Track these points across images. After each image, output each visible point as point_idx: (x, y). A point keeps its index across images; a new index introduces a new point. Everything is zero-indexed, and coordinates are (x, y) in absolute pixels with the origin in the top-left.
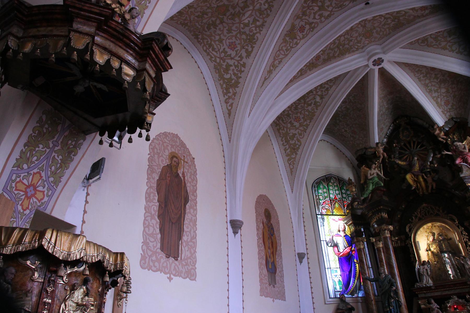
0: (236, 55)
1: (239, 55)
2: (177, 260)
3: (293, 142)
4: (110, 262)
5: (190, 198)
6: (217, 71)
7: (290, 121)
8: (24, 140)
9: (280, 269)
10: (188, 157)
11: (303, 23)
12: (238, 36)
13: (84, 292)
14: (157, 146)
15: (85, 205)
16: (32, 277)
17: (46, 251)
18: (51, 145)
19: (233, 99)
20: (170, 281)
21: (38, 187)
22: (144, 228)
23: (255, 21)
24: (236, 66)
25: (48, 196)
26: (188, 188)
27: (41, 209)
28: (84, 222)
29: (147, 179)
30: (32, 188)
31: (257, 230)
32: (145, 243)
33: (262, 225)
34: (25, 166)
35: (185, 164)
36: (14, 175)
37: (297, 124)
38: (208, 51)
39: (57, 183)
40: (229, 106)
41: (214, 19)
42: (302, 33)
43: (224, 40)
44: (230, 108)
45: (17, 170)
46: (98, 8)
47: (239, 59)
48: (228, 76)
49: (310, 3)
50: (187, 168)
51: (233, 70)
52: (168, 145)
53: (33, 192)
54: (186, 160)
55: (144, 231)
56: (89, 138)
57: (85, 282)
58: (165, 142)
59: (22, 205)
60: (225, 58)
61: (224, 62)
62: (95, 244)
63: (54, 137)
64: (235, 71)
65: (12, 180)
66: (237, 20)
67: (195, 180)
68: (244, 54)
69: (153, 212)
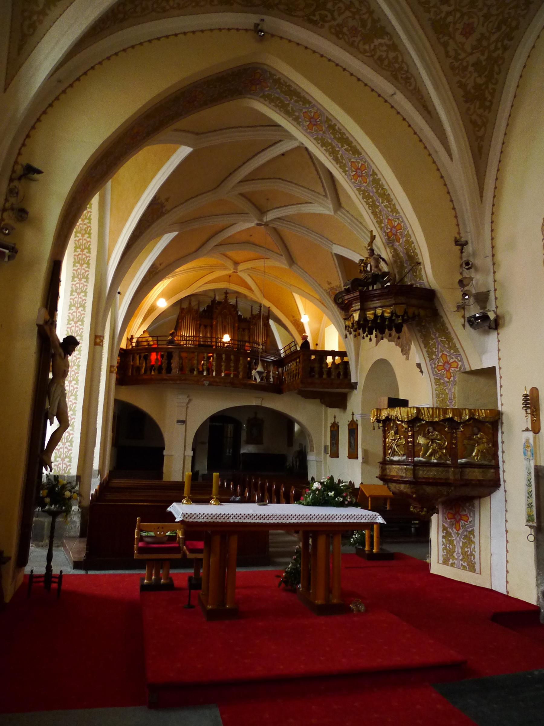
8: (422, 346)
18: (433, 336)
21: (449, 361)
25: (460, 361)
30: (446, 364)
53: (449, 366)
63: (430, 332)
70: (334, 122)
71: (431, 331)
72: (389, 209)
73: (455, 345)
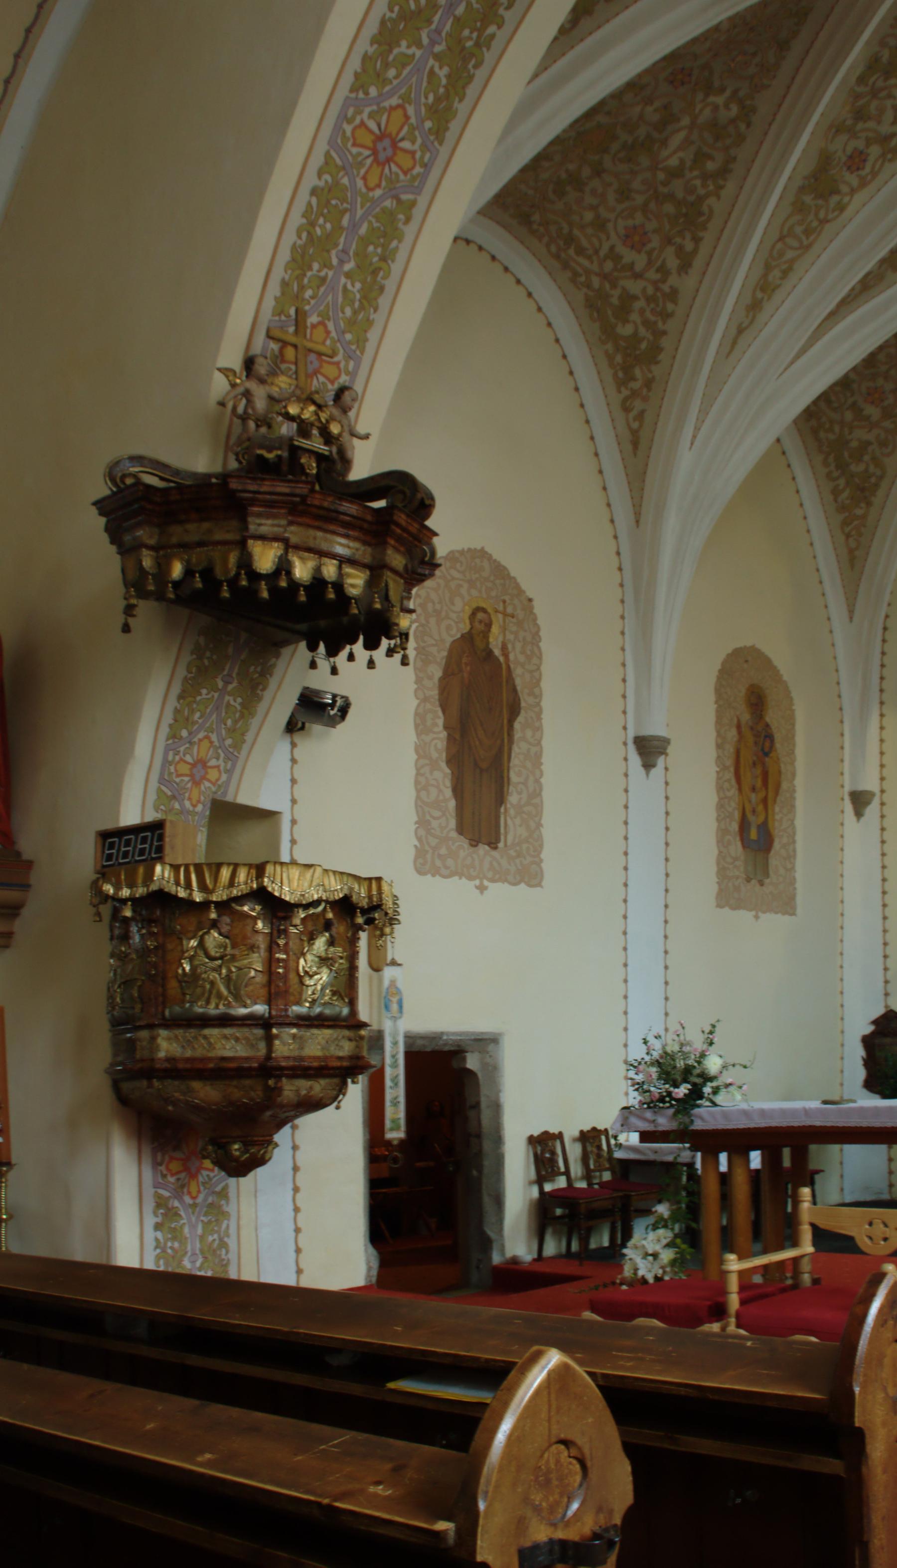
0: (650, 263)
1: (659, 263)
2: (496, 848)
3: (861, 467)
4: (361, 895)
5: (523, 704)
6: (595, 314)
7: (850, 401)
8: (176, 689)
9: (785, 840)
10: (516, 601)
11: (860, 144)
12: (652, 206)
13: (328, 940)
14: (433, 595)
15: (292, 768)
16: (254, 927)
17: (271, 895)
18: (220, 684)
19: (645, 399)
20: (482, 893)
21: (209, 761)
22: (418, 791)
23: (700, 157)
24: (649, 299)
26: (518, 682)
27: (218, 797)
28: (294, 801)
29: (416, 683)
30: (199, 766)
31: (719, 746)
32: (422, 823)
33: (734, 732)
34: (184, 733)
35: (507, 621)
36: (171, 753)
37: (874, 412)
38: (563, 255)
39: (237, 746)
40: (635, 420)
41: (571, 167)
42: (855, 173)
43: (609, 221)
44: (635, 425)
45: (174, 742)
46: (287, 485)
47: (658, 276)
48: (626, 330)
49: (877, 79)
50: (514, 629)
51: (642, 312)
52: (461, 582)
54: (509, 610)
55: (418, 798)
56: (286, 651)
57: (328, 926)
58: (453, 579)
59: (190, 799)
60: (616, 274)
61: (614, 286)
62: (334, 872)
63: (223, 669)
64: (648, 314)
65: (170, 762)
66: (645, 161)
67: (534, 653)
68: (673, 263)
69: (435, 755)
70: (508, 15)
71: (227, 668)
72: (348, 312)
73: (247, 731)
